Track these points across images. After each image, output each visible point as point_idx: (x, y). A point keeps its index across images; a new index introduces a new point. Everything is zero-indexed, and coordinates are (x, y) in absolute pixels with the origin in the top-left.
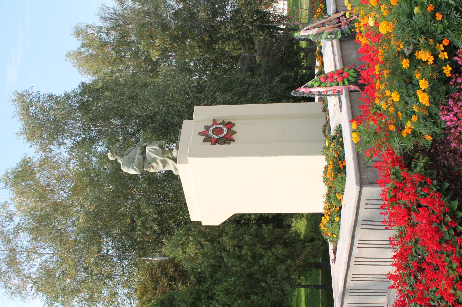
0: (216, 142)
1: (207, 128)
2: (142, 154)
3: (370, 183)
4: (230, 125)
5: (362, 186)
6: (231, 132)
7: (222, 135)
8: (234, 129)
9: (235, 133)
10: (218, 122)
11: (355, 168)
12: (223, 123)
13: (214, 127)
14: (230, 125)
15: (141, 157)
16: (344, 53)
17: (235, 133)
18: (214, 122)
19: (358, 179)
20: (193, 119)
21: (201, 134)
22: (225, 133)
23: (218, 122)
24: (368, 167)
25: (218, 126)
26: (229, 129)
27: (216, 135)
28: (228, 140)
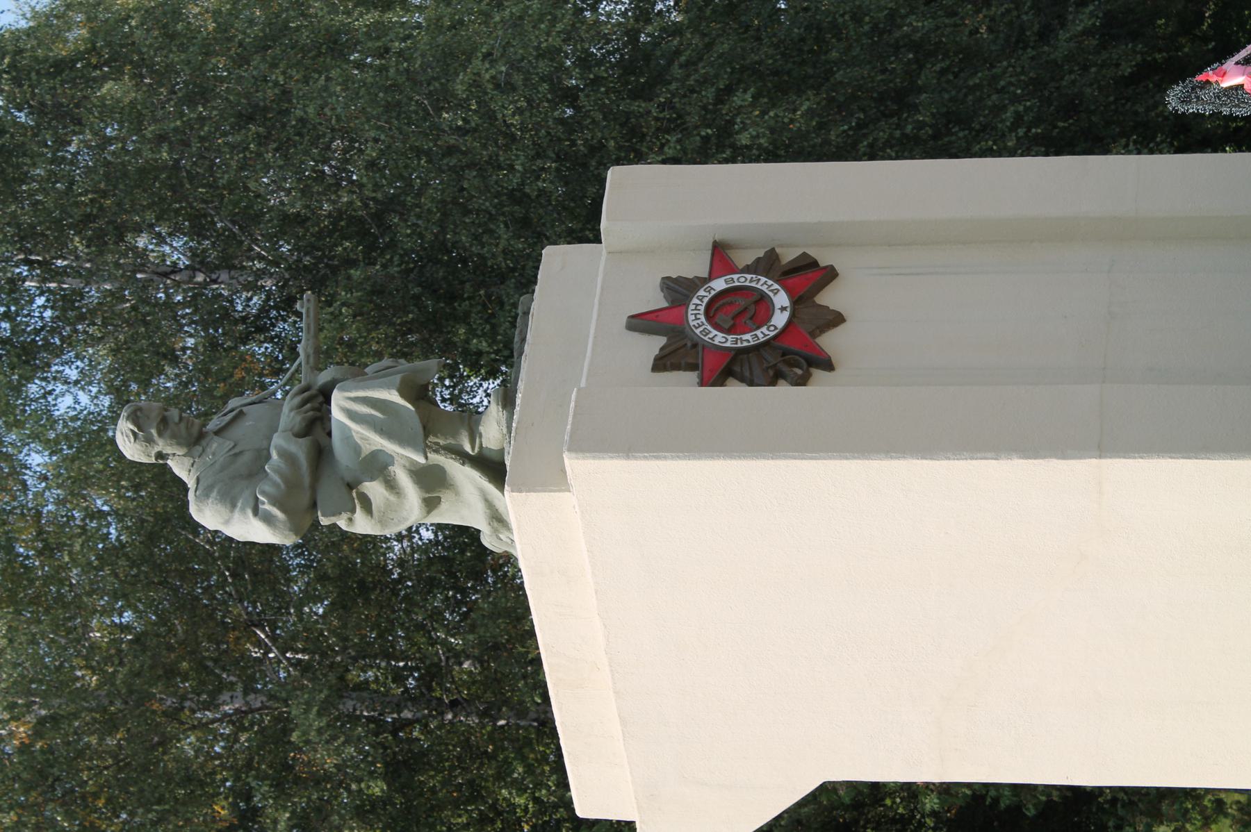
4: (806, 275)
6: (815, 319)
7: (763, 334)
8: (830, 298)
12: (768, 264)
13: (719, 285)
14: (806, 275)
15: (299, 449)
18: (721, 256)
20: (598, 240)
21: (641, 323)
22: (780, 319)
23: (744, 258)
25: (739, 280)
26: (800, 301)
27: (729, 331)
28: (795, 358)
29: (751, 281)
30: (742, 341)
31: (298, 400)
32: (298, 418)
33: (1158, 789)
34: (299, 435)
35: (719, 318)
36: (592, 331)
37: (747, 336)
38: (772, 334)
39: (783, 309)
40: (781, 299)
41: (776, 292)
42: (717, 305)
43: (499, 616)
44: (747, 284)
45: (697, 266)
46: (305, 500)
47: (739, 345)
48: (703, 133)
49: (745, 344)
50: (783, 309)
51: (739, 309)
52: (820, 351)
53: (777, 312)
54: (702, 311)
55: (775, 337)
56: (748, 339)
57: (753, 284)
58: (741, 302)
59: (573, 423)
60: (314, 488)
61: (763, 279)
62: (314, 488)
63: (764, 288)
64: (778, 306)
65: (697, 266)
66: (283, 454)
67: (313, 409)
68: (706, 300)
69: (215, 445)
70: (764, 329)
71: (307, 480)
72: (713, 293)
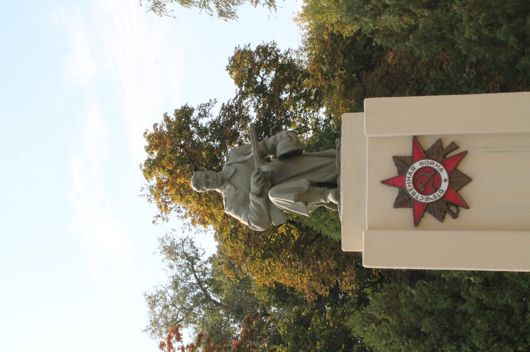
4: (448, 154)
6: (459, 180)
13: (417, 166)
28: (450, 206)
29: (431, 164)
30: (429, 199)
31: (256, 180)
32: (258, 188)
36: (365, 123)
37: (431, 196)
38: (442, 195)
39: (445, 180)
41: (441, 170)
42: (417, 177)
44: (429, 165)
45: (407, 150)
46: (267, 219)
47: (428, 201)
49: (431, 201)
50: (445, 180)
51: (427, 181)
53: (443, 182)
54: (411, 181)
55: (443, 197)
57: (431, 166)
58: (429, 175)
59: (365, 237)
60: (269, 214)
61: (436, 163)
62: (269, 214)
63: (436, 168)
64: (443, 179)
66: (255, 204)
67: (262, 182)
68: (412, 175)
69: (228, 187)
70: (438, 192)
71: (266, 212)
72: (415, 170)
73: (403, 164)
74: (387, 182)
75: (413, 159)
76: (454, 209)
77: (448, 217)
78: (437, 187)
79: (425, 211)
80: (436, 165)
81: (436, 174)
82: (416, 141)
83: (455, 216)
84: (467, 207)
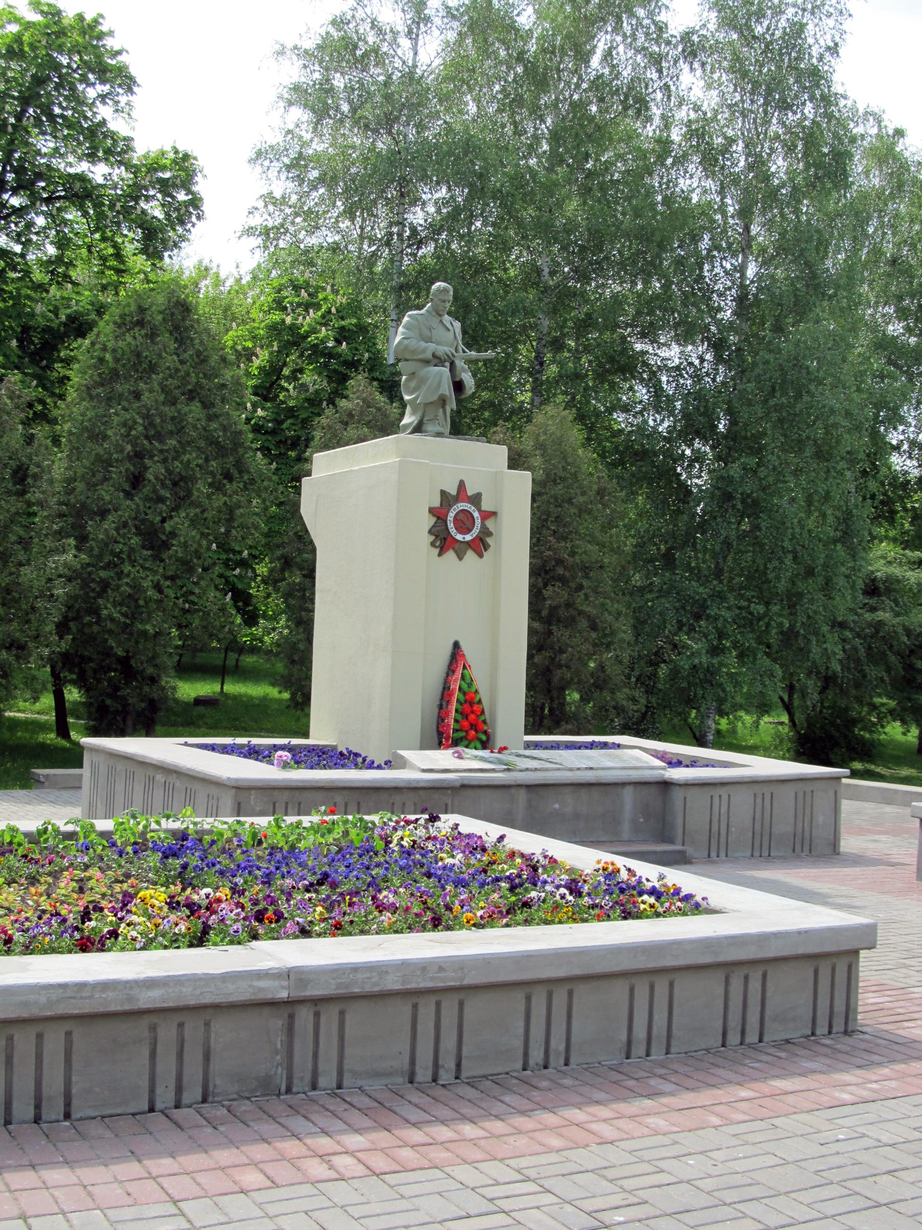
0: (439, 514)
1: (476, 500)
2: (434, 355)
3: (239, 804)
4: (480, 545)
5: (234, 791)
6: (460, 550)
7: (453, 531)
8: (470, 555)
9: (460, 558)
10: (490, 523)
11: (304, 781)
12: (486, 532)
13: (476, 514)
14: (480, 545)
15: (428, 355)
16: (568, 789)
17: (460, 558)
18: (487, 515)
19: (246, 784)
20: (510, 467)
21: (462, 485)
22: (459, 537)
23: (490, 523)
24: (274, 804)
25: (478, 522)
26: (469, 544)
27: (455, 518)
28: (442, 541)
33: (309, 678)
34: (434, 355)
35: (461, 515)
40: (468, 538)
43: (810, 268)
45: (486, 506)
48: (361, 496)
52: (447, 550)
56: (451, 526)
65: (486, 506)
73: (476, 500)
74: (462, 485)
75: (480, 511)
76: (438, 544)
77: (433, 538)
78: (461, 530)
79: (438, 518)
80: (475, 532)
81: (469, 531)
82: (494, 514)
83: (433, 544)
84: (440, 555)
